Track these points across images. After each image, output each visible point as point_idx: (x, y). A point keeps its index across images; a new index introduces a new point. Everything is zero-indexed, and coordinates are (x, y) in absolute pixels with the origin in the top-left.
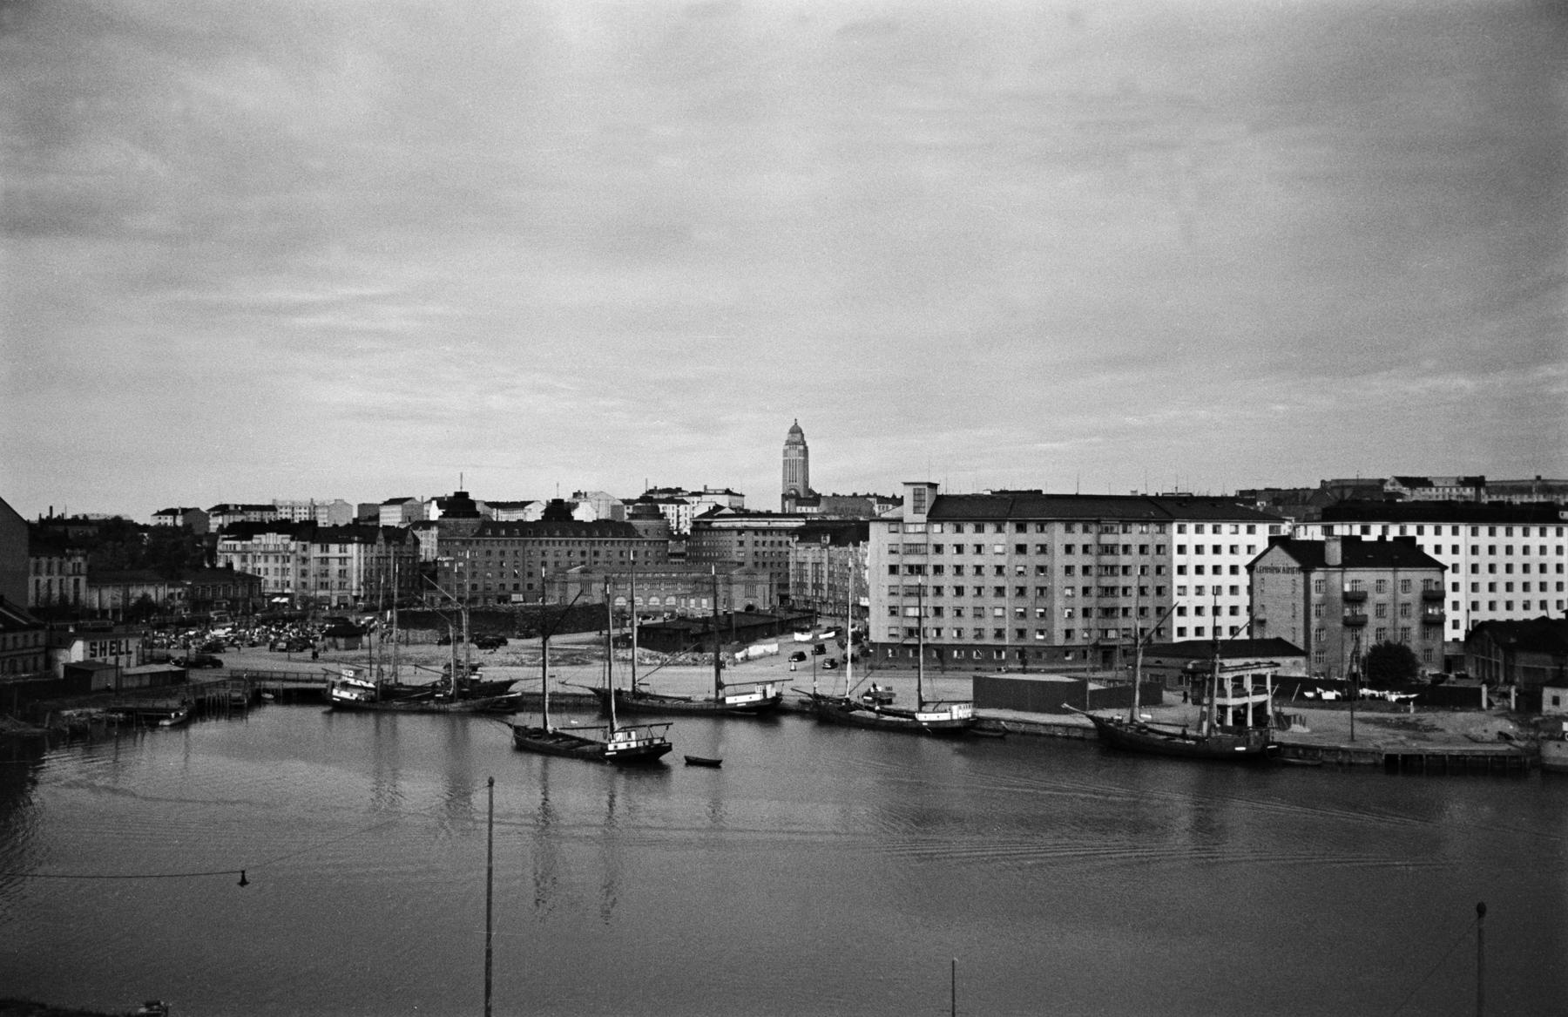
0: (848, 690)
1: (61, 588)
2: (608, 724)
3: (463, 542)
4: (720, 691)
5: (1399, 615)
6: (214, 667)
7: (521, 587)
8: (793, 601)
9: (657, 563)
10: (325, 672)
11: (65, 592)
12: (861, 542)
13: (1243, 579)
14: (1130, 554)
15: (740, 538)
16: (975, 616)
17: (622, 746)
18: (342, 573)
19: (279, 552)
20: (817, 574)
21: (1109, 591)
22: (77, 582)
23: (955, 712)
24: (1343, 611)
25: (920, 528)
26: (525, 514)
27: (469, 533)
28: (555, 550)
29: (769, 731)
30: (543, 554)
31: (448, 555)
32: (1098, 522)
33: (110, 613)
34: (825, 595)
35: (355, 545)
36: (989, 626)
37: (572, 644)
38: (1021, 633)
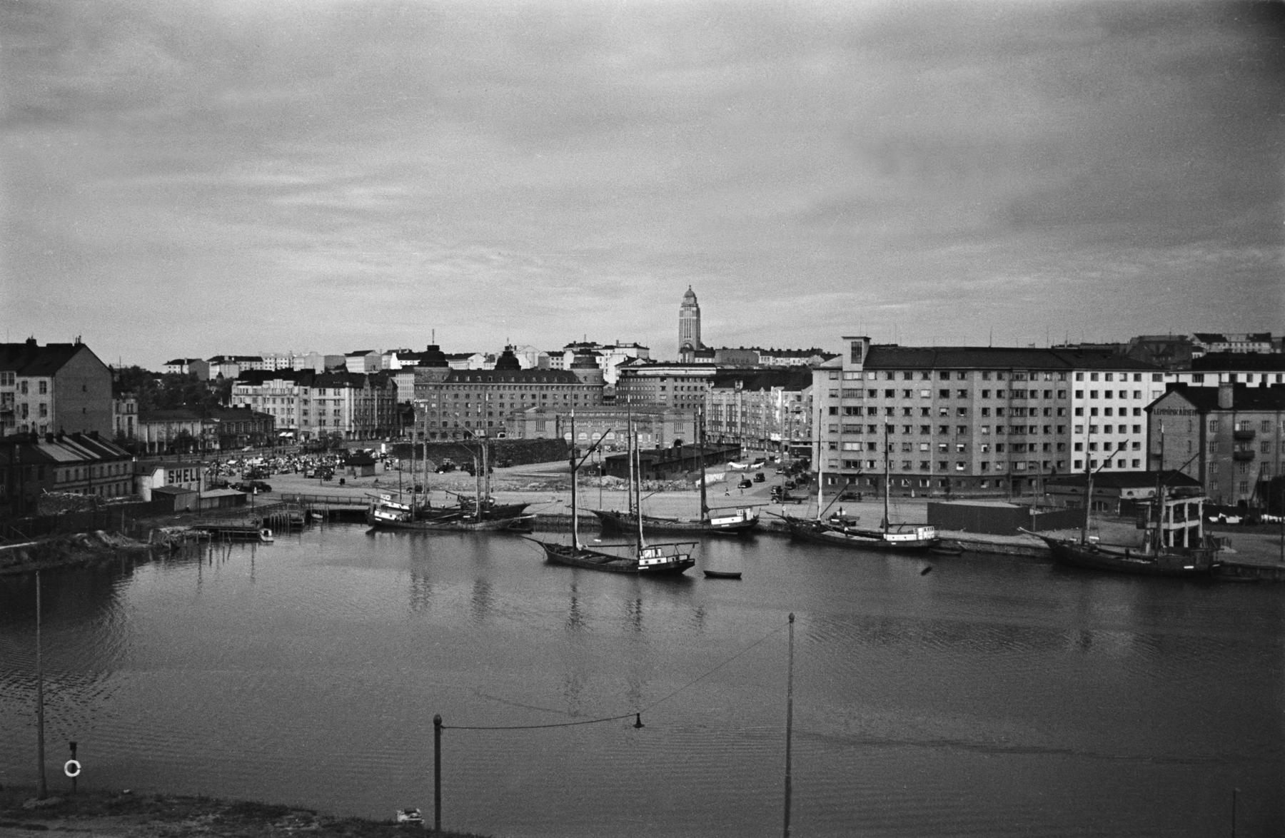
1: (118, 425)
2: (636, 542)
3: (436, 387)
4: (705, 514)
5: (1281, 451)
6: (264, 491)
8: (709, 436)
9: (594, 404)
11: (121, 428)
12: (772, 388)
13: (1142, 420)
14: (1037, 398)
15: (662, 384)
16: (904, 450)
18: (337, 412)
20: (732, 414)
21: (1019, 429)
22: (130, 419)
23: (920, 534)
24: (1234, 448)
25: (856, 376)
26: (469, 364)
27: (440, 378)
28: (509, 394)
29: (749, 550)
30: (501, 397)
31: (423, 397)
32: (1010, 371)
33: (157, 445)
35: (347, 389)
37: (551, 472)
38: (944, 465)
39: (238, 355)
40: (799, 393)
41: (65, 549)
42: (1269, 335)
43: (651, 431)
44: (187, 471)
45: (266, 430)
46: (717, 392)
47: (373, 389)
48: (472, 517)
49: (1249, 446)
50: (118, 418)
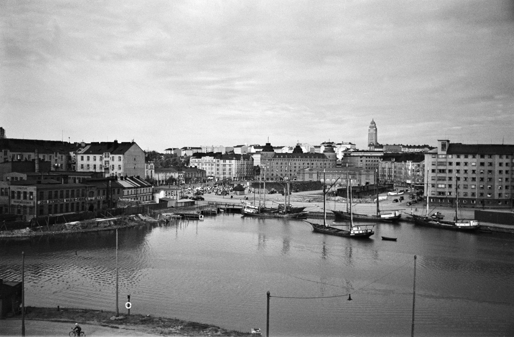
0: (427, 214)
1: (147, 173)
2: (350, 224)
3: (269, 160)
6: (202, 200)
8: (380, 181)
9: (333, 167)
12: (407, 161)
15: (361, 159)
17: (357, 232)
18: (230, 169)
19: (210, 162)
20: (390, 171)
22: (151, 171)
25: (444, 156)
28: (298, 163)
31: (264, 164)
32: (512, 155)
34: (393, 179)
35: (234, 160)
36: (469, 191)
38: (482, 194)
39: (193, 147)
40: (419, 163)
41: (126, 221)
43: (356, 179)
45: (203, 176)
48: (283, 212)
50: (147, 171)
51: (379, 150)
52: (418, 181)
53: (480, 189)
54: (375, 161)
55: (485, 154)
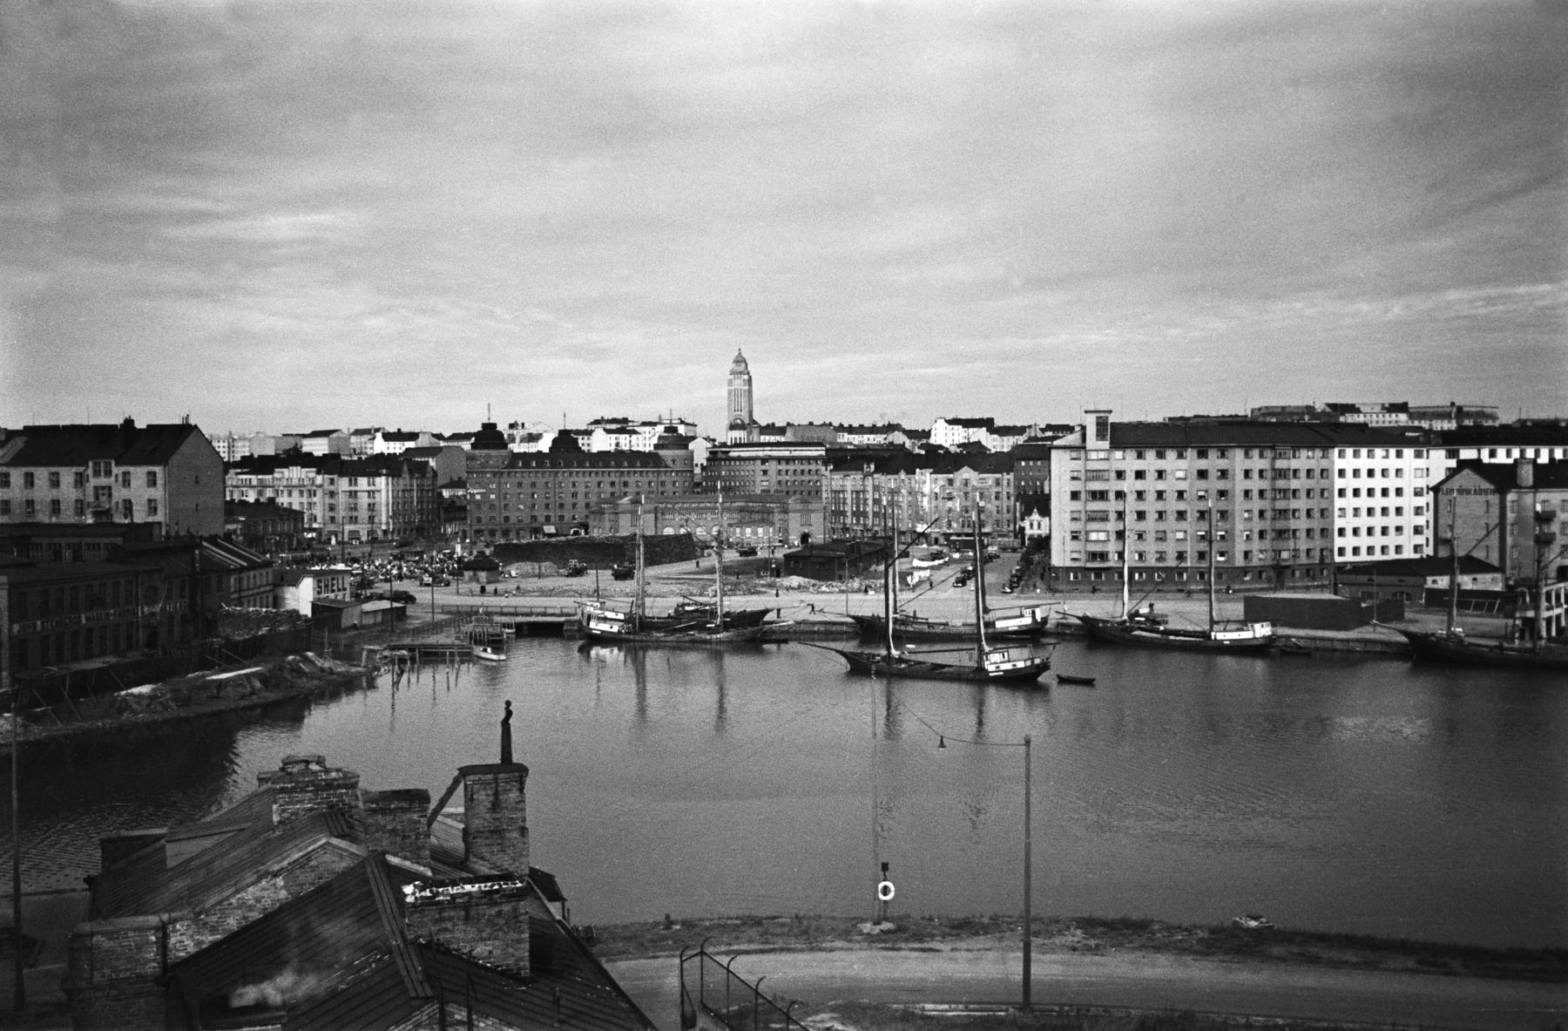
2: (976, 646)
3: (495, 474)
7: (553, 519)
9: (684, 493)
10: (577, 605)
12: (918, 470)
14: (1299, 478)
15: (764, 467)
18: (371, 507)
19: (305, 486)
21: (1283, 513)
24: (1534, 530)
25: (1102, 455)
27: (500, 464)
28: (583, 485)
31: (481, 487)
32: (1273, 448)
35: (383, 478)
36: (1171, 549)
40: (951, 476)
42: (1405, 404)
43: (772, 524)
44: (333, 579)
46: (837, 476)
47: (412, 477)
49: (1549, 528)
51: (773, 439)
52: (950, 526)
53: (1198, 541)
54: (803, 471)
55: (1210, 447)
